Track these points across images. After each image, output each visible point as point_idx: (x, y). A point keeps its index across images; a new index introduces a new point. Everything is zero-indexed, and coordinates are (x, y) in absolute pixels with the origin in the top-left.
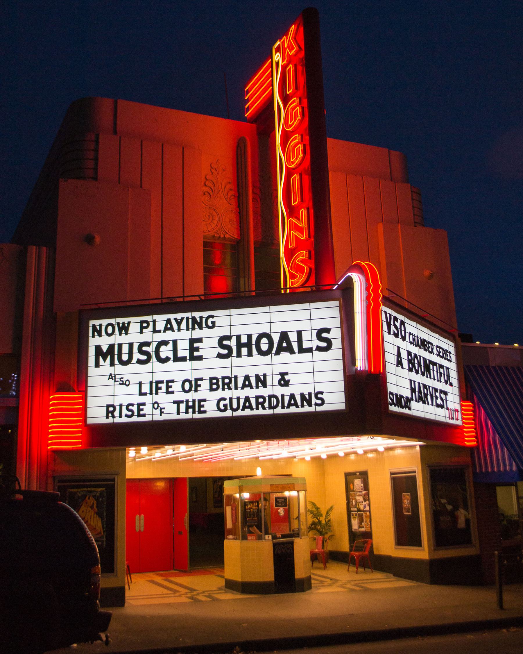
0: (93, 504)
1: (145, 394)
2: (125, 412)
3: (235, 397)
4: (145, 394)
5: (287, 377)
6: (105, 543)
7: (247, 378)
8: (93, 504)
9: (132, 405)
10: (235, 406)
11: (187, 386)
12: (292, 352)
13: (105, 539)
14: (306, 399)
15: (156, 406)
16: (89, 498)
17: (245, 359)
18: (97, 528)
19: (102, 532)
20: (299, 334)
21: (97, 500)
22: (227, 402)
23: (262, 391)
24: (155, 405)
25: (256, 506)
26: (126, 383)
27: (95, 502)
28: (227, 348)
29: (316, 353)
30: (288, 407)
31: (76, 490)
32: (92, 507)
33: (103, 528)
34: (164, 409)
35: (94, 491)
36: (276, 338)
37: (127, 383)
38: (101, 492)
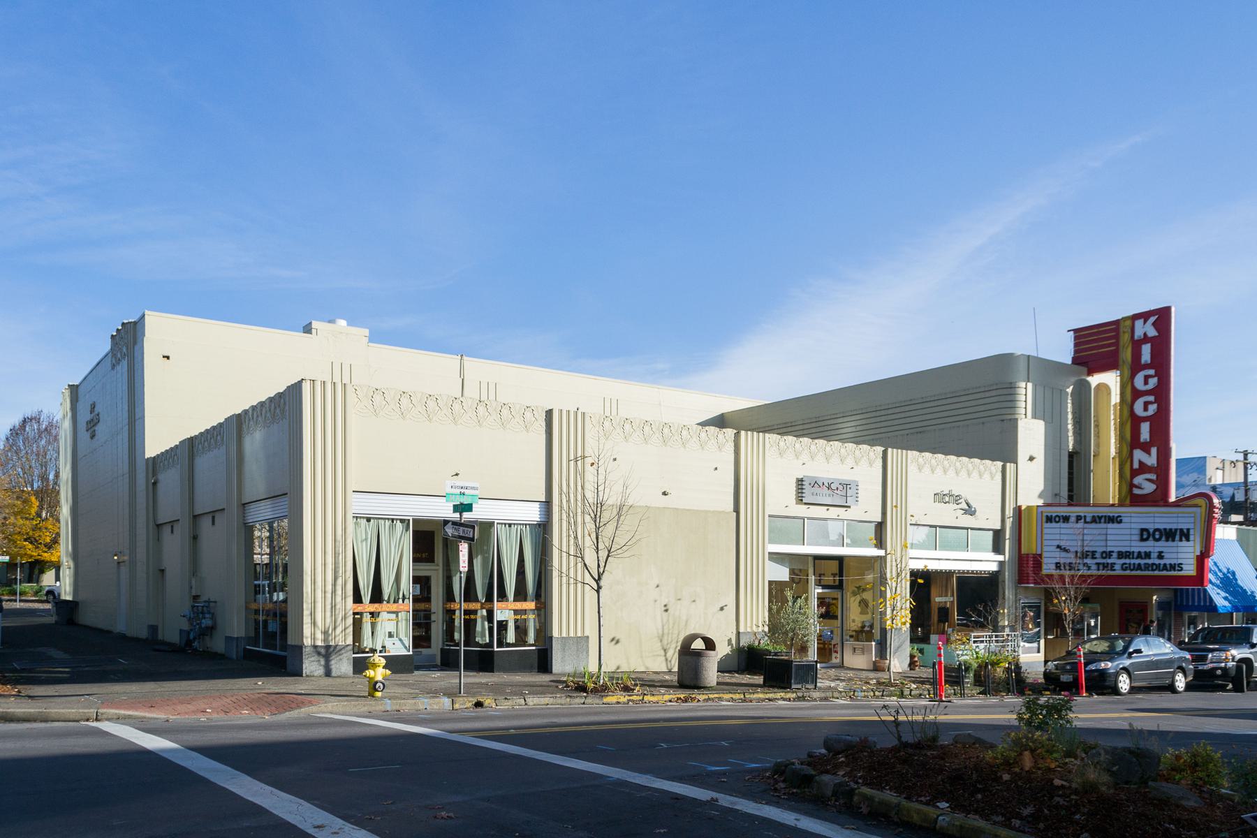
14: (1173, 567)
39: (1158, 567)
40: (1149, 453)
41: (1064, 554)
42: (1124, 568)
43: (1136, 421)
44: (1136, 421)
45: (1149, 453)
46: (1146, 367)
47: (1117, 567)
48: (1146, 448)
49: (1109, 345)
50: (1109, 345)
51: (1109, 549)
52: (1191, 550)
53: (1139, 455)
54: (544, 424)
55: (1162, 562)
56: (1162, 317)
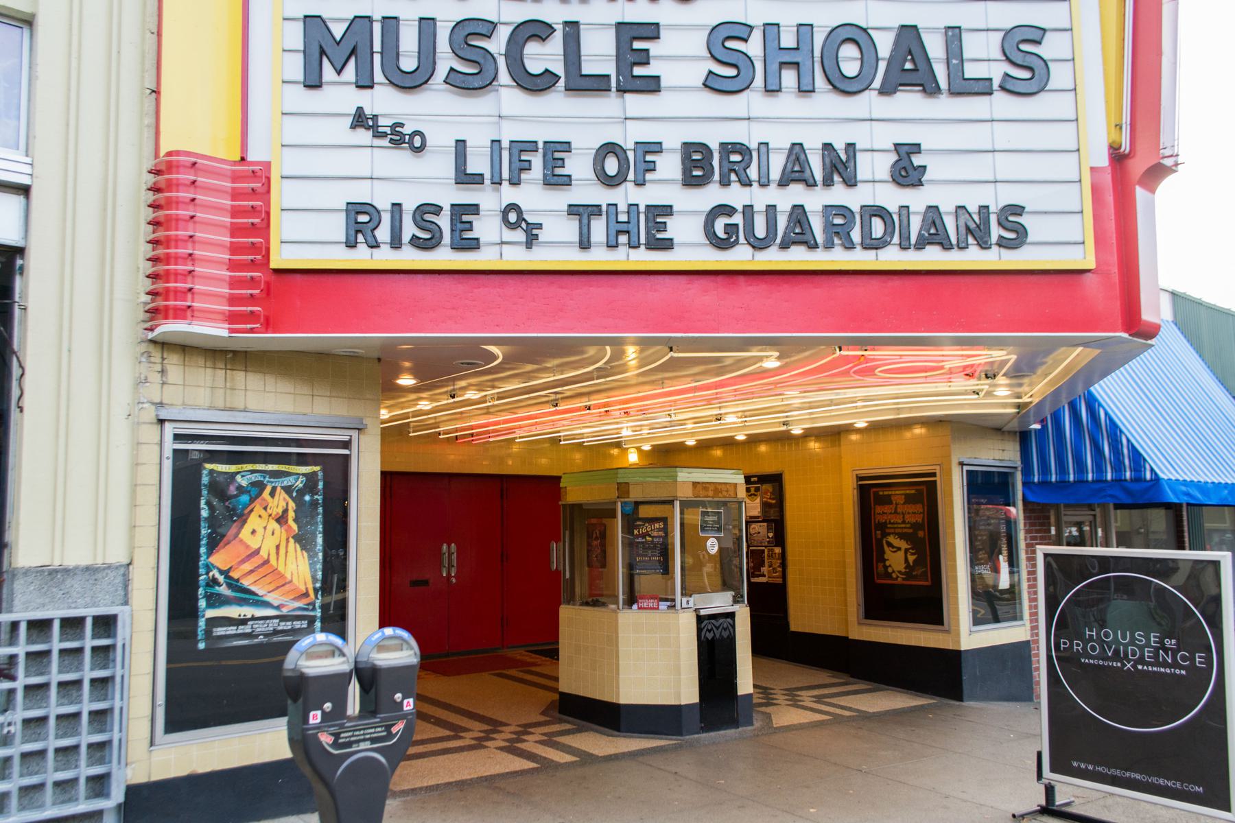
0: (286, 511)
1: (477, 179)
2: (409, 229)
4: (477, 179)
5: (917, 160)
7: (797, 152)
8: (286, 511)
9: (437, 210)
10: (760, 231)
11: (612, 166)
12: (930, 88)
13: (318, 613)
15: (513, 217)
16: (272, 494)
17: (788, 103)
18: (295, 581)
19: (311, 593)
20: (954, 35)
21: (298, 501)
22: (737, 219)
23: (838, 195)
24: (513, 216)
25: (659, 530)
27: (292, 505)
29: (999, 97)
30: (920, 245)
31: (232, 468)
32: (281, 519)
33: (314, 579)
34: (539, 226)
35: (288, 474)
36: (885, 45)
37: (417, 141)
38: (311, 478)
41: (398, 161)
47: (685, 230)
51: (989, 381)
52: (1063, 136)
54: (433, 696)
55: (917, 200)
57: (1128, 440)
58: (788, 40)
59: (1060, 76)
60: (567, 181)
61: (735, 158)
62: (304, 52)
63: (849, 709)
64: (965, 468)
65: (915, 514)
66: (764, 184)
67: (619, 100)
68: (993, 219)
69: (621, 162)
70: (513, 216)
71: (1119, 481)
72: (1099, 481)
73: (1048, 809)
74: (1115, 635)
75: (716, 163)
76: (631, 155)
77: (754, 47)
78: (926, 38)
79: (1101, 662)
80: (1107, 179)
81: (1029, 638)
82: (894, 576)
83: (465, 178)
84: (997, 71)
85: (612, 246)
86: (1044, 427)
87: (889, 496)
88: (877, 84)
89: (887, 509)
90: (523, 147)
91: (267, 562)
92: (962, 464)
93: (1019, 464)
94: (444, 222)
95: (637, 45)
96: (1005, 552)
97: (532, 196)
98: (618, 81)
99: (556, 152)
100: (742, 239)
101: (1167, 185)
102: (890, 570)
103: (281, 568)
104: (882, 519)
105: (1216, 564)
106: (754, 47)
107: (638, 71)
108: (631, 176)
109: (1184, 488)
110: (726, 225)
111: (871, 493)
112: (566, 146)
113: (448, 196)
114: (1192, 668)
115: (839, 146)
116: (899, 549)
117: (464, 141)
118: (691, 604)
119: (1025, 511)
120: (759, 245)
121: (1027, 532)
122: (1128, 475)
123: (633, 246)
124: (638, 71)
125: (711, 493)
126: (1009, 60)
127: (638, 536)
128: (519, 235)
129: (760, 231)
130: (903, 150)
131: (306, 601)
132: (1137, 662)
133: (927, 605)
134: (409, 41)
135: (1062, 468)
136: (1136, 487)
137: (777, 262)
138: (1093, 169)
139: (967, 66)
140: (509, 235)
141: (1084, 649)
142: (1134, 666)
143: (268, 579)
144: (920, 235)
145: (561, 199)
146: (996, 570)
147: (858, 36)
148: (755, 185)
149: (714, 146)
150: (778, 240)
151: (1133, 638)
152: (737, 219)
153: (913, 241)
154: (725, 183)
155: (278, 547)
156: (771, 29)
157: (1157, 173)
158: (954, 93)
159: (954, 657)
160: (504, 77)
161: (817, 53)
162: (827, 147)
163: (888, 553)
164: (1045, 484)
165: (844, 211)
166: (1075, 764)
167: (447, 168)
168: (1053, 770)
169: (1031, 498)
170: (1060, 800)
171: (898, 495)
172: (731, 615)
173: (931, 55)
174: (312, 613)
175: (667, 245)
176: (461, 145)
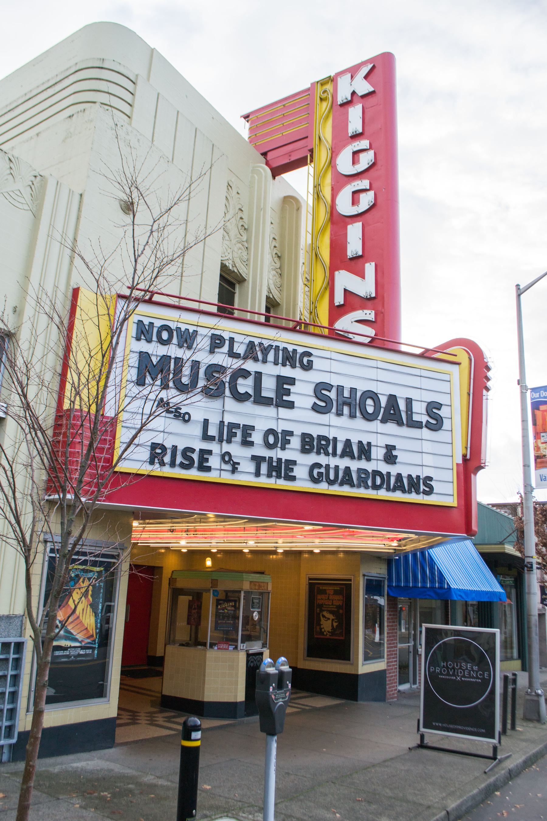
1: (212, 438)
3: (332, 466)
4: (212, 438)
6: (96, 652)
7: (348, 443)
9: (193, 450)
10: (332, 477)
11: (271, 440)
12: (400, 423)
14: (414, 484)
17: (344, 421)
18: (88, 628)
22: (323, 470)
23: (363, 464)
24: (226, 458)
25: (232, 606)
26: (185, 418)
28: (326, 399)
29: (425, 430)
30: (394, 490)
33: (96, 628)
34: (238, 464)
36: (383, 401)
37: (187, 417)
38: (99, 573)
39: (379, 480)
40: (361, 274)
41: (176, 426)
42: (316, 474)
43: (338, 222)
44: (338, 222)
45: (361, 274)
46: (356, 137)
47: (301, 472)
48: (355, 265)
49: (300, 122)
50: (300, 122)
52: (447, 449)
53: (345, 280)
56: (381, 69)
57: (438, 568)
58: (346, 394)
59: (446, 424)
60: (251, 444)
61: (323, 442)
62: (138, 368)
63: (307, 706)
64: (366, 578)
65: (338, 600)
66: (334, 454)
67: (275, 410)
68: (421, 481)
69: (278, 438)
70: (226, 458)
71: (432, 588)
72: (415, 587)
73: (422, 746)
74: (454, 664)
75: (315, 443)
76: (280, 435)
77: (333, 395)
78: (399, 400)
79: (447, 677)
80: (461, 468)
81: (386, 668)
82: (325, 633)
83: (206, 437)
84: (424, 419)
85: (269, 476)
86: (400, 558)
87: (325, 590)
88: (380, 417)
89: (323, 596)
90: (233, 426)
91: (78, 617)
92: (364, 575)
93: (386, 577)
94: (195, 456)
95: (285, 386)
96: (378, 622)
97: (235, 449)
98: (276, 401)
99: (247, 430)
100: (324, 480)
101: (481, 473)
102: (323, 630)
103: (83, 621)
104: (320, 602)
105: (494, 634)
106: (333, 395)
107: (285, 398)
108: (279, 445)
109: (459, 593)
110: (318, 472)
111: (316, 587)
112: (253, 428)
113: (199, 445)
114: (483, 679)
115: (365, 442)
116: (329, 619)
117: (208, 420)
118: (245, 648)
119: (388, 600)
120: (331, 483)
121: (388, 611)
122: (437, 585)
123: (279, 477)
124: (285, 398)
125: (257, 587)
126: (429, 415)
127: (220, 609)
128: (229, 467)
129: (332, 477)
130: (389, 448)
131: (92, 639)
132: (462, 677)
133: (341, 649)
134: (186, 370)
135: (407, 580)
136: (440, 591)
137: (338, 491)
138: (457, 464)
139: (414, 415)
140: (224, 467)
141: (441, 671)
142: (461, 679)
143: (78, 627)
144: (394, 486)
145: (248, 452)
146: (374, 632)
147: (373, 396)
148: (331, 455)
149: (315, 436)
150: (339, 481)
151: (461, 666)
152: (323, 470)
153: (392, 487)
154: (318, 453)
155: (83, 610)
156: (340, 389)
157: (480, 467)
158: (409, 426)
159: (354, 678)
160: (227, 392)
161: (358, 402)
162: (360, 442)
163: (323, 620)
164: (398, 587)
165: (365, 471)
166: (434, 724)
167: (198, 431)
168: (425, 727)
169: (391, 594)
170: (427, 741)
171: (330, 590)
172: (261, 654)
173: (401, 409)
174: (94, 646)
175: (293, 478)
176: (206, 422)
